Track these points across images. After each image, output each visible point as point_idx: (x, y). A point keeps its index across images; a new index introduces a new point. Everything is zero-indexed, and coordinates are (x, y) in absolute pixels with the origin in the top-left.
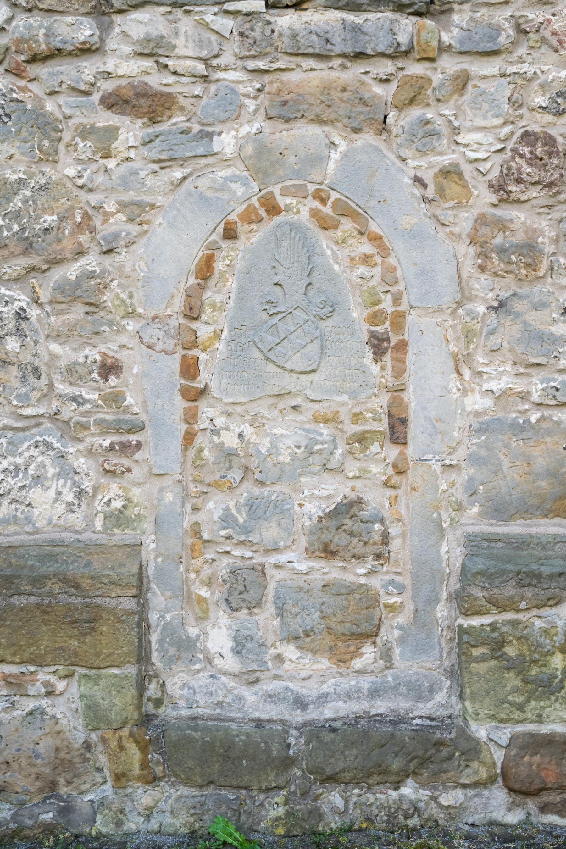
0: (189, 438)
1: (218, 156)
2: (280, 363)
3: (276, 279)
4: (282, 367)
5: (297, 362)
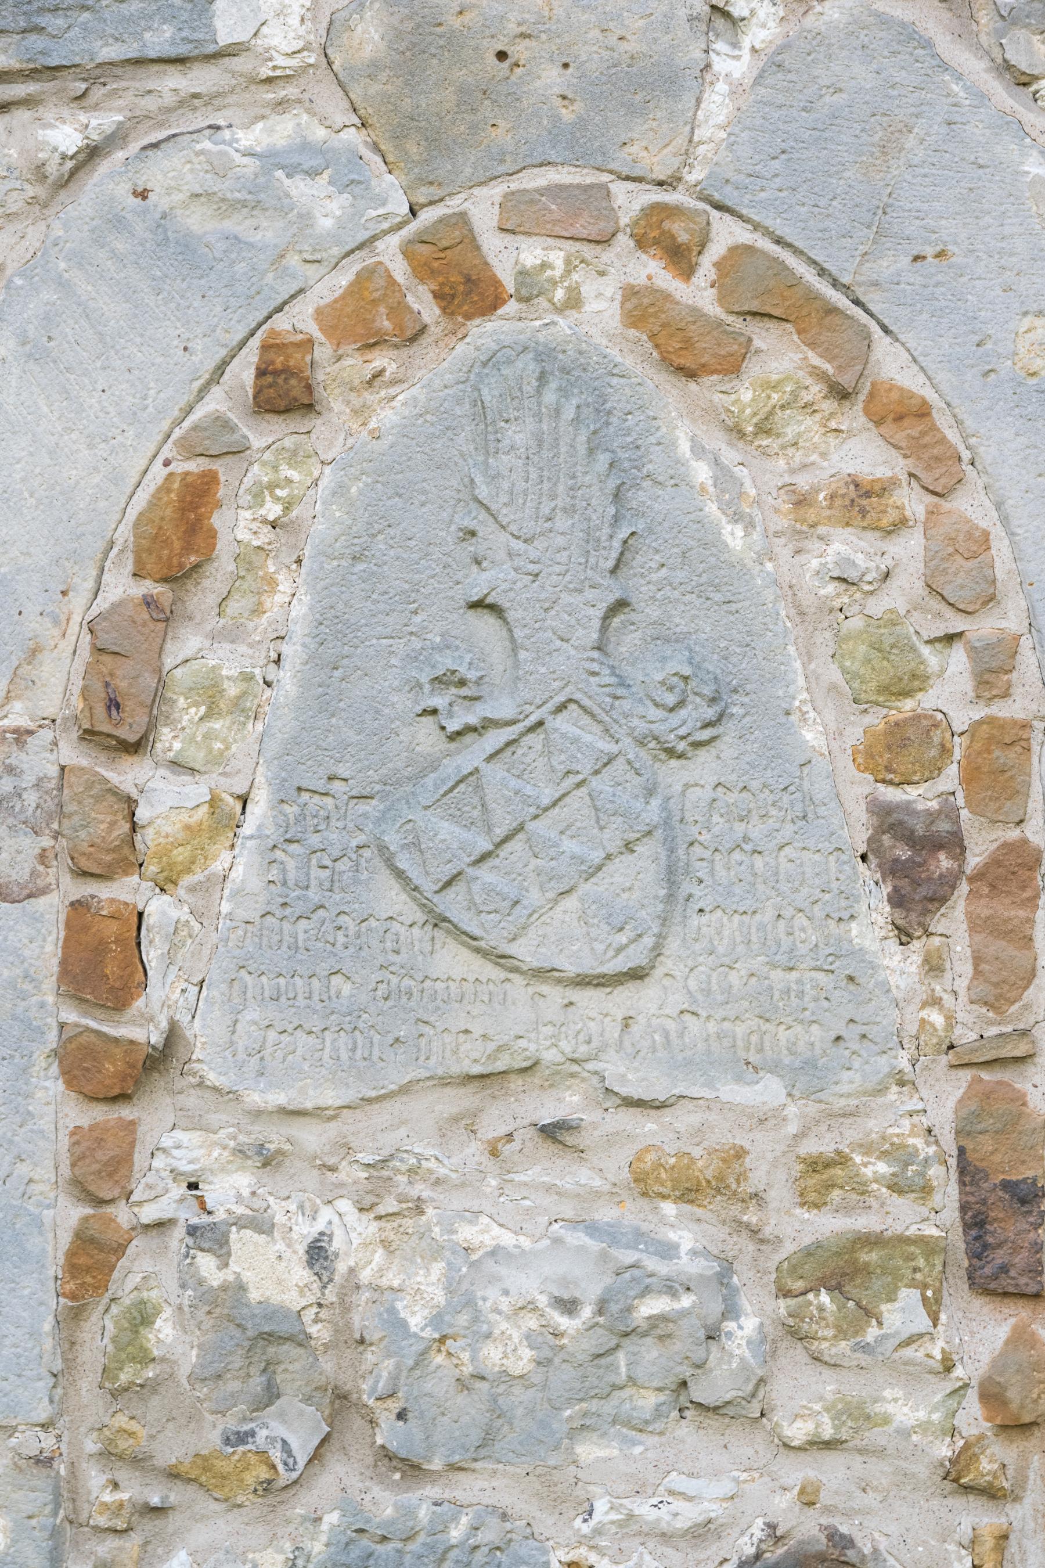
0: (92, 1261)
1: (236, 63)
2: (493, 940)
3: (479, 584)
4: (500, 958)
5: (562, 934)
